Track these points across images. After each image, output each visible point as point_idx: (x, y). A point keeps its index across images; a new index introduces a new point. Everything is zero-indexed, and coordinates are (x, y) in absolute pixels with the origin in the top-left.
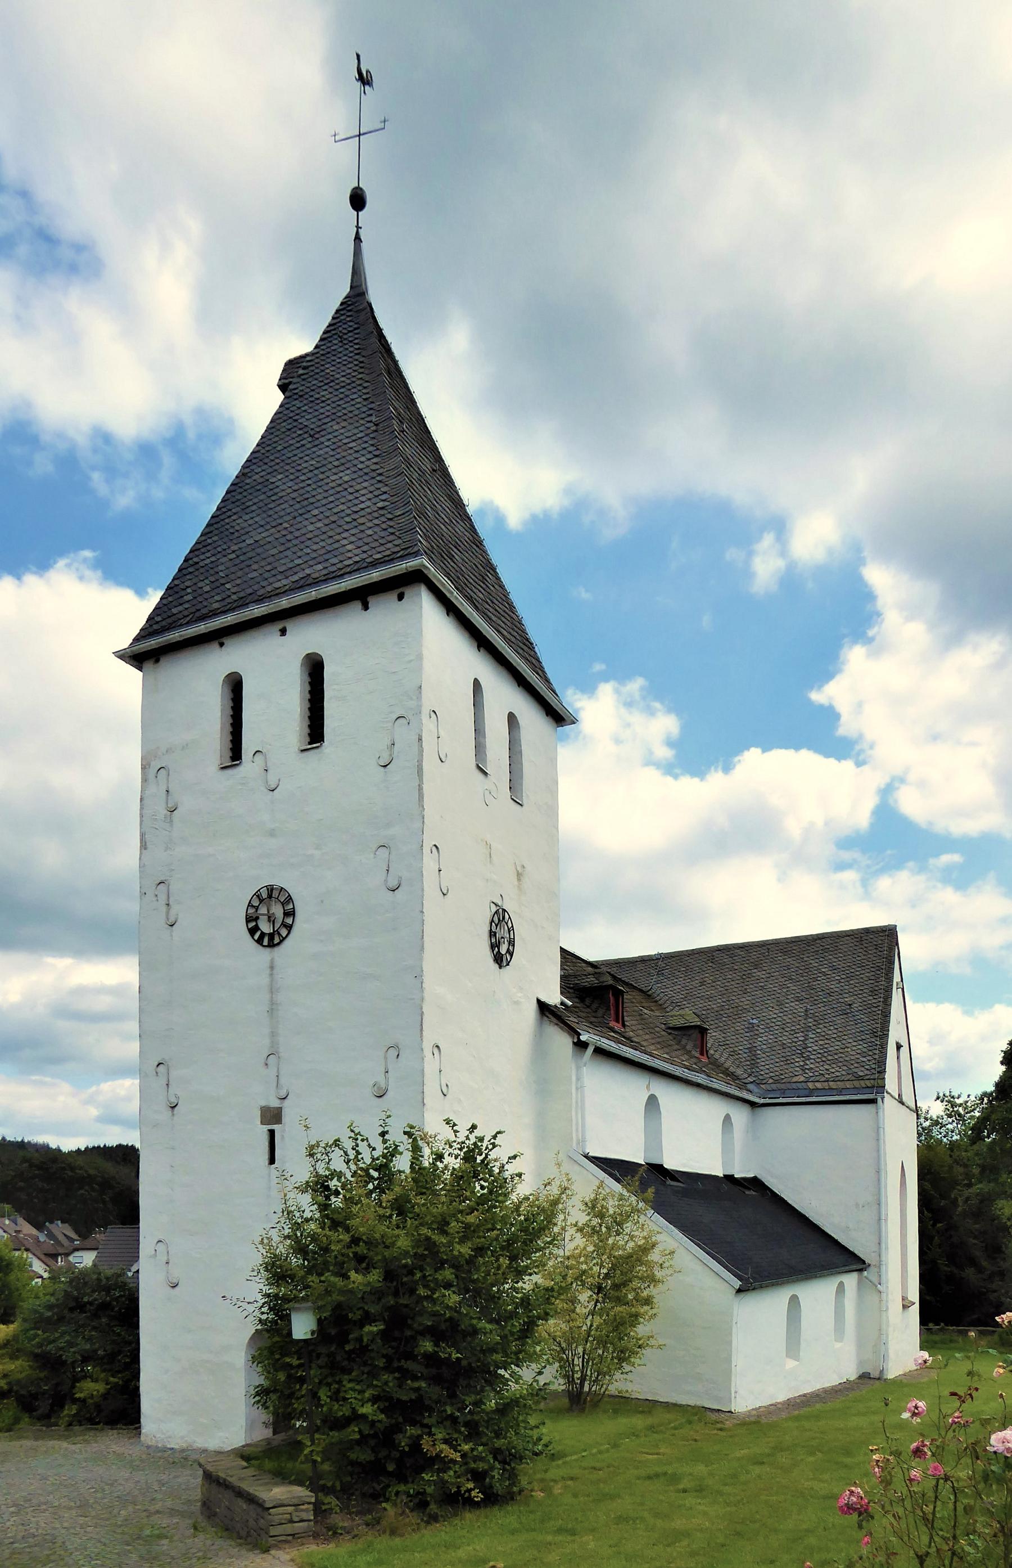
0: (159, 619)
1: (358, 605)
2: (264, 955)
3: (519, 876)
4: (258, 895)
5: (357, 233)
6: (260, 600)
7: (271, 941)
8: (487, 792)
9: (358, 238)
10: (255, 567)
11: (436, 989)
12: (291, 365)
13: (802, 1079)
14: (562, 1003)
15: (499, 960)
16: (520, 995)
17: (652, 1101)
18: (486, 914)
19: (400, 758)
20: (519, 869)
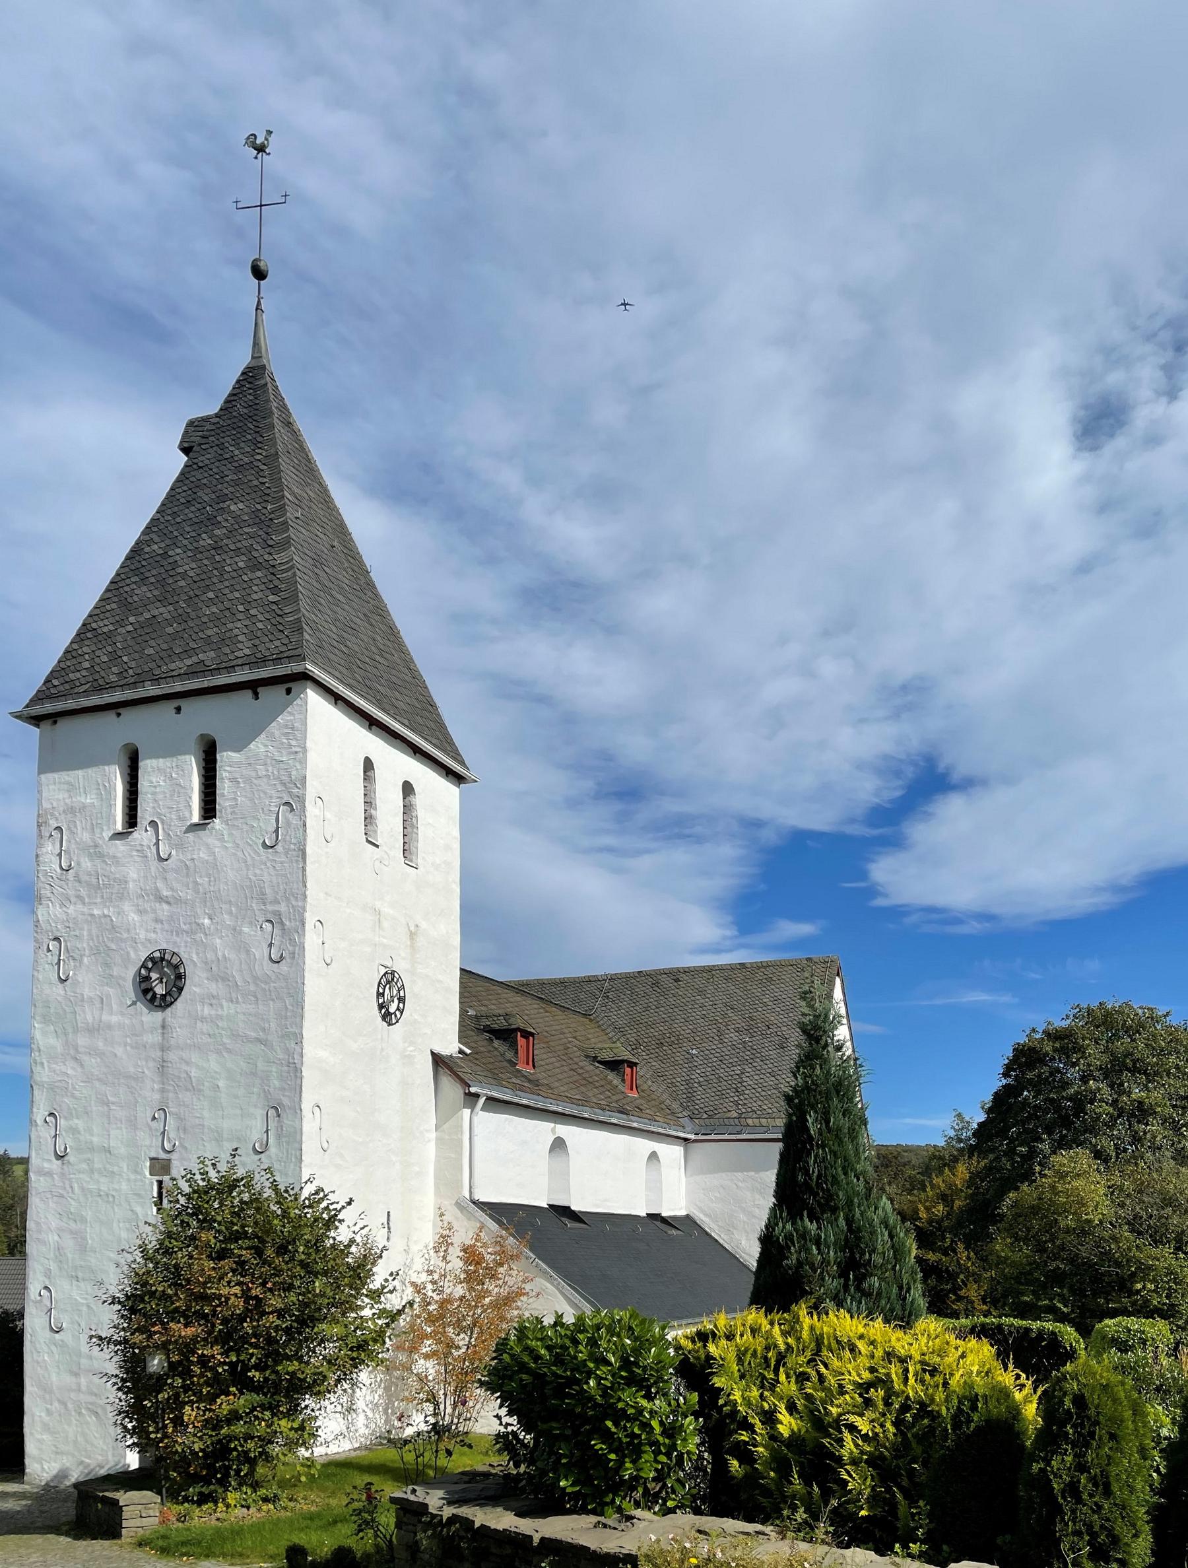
0: (56, 682)
1: (248, 694)
3: (412, 935)
5: (259, 303)
6: (156, 680)
7: (161, 1003)
8: (377, 863)
10: (152, 643)
12: (193, 425)
13: (735, 1115)
14: (461, 1052)
15: (387, 1017)
16: (411, 1048)
17: (559, 1144)
18: (377, 973)
19: (286, 843)
20: (412, 928)
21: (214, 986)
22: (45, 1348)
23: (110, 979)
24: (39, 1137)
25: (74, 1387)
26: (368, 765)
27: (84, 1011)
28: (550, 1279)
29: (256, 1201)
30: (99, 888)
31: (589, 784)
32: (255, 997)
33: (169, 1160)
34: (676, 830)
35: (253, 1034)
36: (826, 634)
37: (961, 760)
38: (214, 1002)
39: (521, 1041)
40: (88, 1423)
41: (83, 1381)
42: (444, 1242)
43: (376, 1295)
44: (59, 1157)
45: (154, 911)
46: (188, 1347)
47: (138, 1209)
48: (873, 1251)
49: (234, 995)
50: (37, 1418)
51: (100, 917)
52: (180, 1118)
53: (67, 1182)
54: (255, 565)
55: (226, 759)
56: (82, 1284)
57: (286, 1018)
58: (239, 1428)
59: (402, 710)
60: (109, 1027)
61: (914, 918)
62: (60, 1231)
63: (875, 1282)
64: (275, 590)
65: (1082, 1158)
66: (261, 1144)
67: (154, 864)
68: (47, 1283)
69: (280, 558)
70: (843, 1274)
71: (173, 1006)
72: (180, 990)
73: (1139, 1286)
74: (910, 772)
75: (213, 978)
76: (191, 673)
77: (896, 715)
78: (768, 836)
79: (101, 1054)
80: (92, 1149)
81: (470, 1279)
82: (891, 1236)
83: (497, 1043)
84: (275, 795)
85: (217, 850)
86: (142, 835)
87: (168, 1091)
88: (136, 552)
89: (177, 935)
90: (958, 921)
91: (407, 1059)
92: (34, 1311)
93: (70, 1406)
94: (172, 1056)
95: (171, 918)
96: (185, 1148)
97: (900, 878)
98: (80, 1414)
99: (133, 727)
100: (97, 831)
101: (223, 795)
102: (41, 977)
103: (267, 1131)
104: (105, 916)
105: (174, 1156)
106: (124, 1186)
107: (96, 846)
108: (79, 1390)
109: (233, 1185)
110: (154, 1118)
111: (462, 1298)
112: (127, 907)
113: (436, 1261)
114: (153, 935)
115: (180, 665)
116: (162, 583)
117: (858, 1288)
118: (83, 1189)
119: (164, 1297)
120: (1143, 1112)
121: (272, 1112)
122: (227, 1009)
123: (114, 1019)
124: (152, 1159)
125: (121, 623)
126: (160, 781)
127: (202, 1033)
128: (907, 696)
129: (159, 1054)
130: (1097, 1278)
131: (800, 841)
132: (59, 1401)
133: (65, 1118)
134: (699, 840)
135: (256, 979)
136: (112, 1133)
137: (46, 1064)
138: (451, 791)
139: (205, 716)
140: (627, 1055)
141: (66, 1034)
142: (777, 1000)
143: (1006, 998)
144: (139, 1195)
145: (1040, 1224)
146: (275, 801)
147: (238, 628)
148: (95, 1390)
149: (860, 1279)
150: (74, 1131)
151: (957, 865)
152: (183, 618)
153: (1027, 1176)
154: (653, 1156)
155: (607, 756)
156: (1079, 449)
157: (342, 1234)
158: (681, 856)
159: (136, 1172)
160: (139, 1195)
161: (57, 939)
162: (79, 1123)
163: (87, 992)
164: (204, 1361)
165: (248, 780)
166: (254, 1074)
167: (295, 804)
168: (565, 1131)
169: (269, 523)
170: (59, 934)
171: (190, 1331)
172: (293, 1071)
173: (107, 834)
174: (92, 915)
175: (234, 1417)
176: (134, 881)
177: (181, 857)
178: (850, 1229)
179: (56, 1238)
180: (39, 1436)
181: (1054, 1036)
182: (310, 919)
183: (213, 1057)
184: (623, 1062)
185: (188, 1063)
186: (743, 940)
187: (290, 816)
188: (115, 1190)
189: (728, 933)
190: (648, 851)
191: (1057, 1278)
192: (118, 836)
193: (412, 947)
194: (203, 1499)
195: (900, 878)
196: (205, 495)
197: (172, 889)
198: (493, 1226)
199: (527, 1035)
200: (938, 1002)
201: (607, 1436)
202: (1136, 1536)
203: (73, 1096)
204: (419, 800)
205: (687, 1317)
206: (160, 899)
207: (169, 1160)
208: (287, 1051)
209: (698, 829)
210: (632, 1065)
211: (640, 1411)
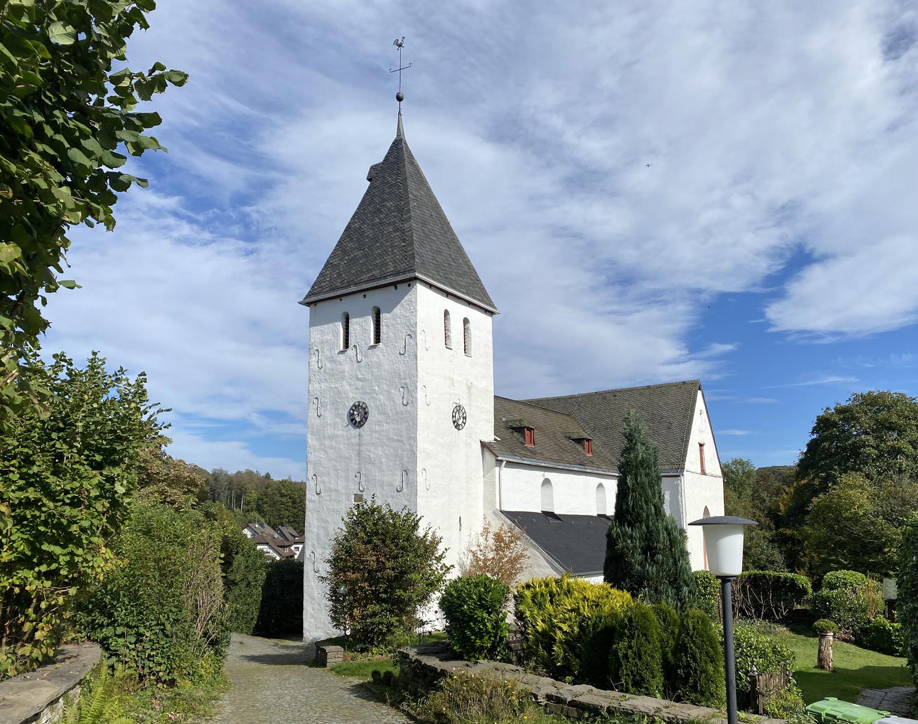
1: (393, 288)
2: (354, 432)
3: (469, 388)
4: (354, 405)
6: (356, 284)
7: (357, 424)
9: (399, 113)
11: (424, 442)
15: (457, 427)
17: (547, 482)
19: (409, 353)
23: (338, 415)
26: (446, 313)
28: (537, 549)
29: (382, 518)
31: (604, 278)
34: (652, 299)
36: (736, 183)
37: (818, 245)
39: (527, 432)
42: (486, 531)
43: (439, 559)
44: (318, 494)
46: (353, 583)
48: (658, 542)
52: (366, 476)
54: (396, 230)
55: (384, 316)
58: (377, 619)
59: (463, 283)
60: (338, 436)
61: (793, 337)
62: (318, 527)
63: (660, 557)
64: (404, 240)
65: (856, 478)
67: (355, 364)
69: (406, 226)
70: (644, 552)
73: (886, 550)
74: (788, 255)
75: (380, 413)
76: (370, 280)
77: (779, 224)
78: (704, 297)
79: (334, 448)
80: (331, 490)
81: (498, 549)
82: (669, 534)
83: (515, 434)
86: (351, 352)
88: (348, 228)
90: (819, 337)
91: (468, 445)
94: (363, 448)
95: (363, 388)
97: (784, 316)
99: (346, 305)
105: (364, 493)
109: (373, 512)
111: (493, 558)
112: (344, 383)
113: (482, 540)
115: (365, 277)
116: (359, 240)
117: (653, 560)
119: (346, 560)
120: (896, 452)
122: (386, 427)
123: (340, 433)
125: (342, 260)
126: (357, 327)
128: (785, 212)
130: (864, 545)
131: (723, 298)
134: (665, 303)
135: (397, 413)
138: (488, 319)
139: (375, 299)
140: (586, 436)
142: (666, 403)
143: (852, 379)
145: (833, 516)
146: (405, 334)
147: (388, 259)
149: (653, 556)
150: (324, 482)
151: (819, 305)
152: (367, 256)
153: (824, 488)
154: (600, 485)
155: (612, 262)
156: (886, 60)
157: (420, 533)
158: (655, 313)
162: (326, 479)
163: (329, 422)
164: (361, 588)
165: (393, 325)
166: (396, 456)
167: (412, 335)
168: (549, 475)
169: (403, 211)
171: (353, 576)
172: (413, 454)
173: (337, 352)
175: (374, 615)
178: (648, 532)
181: (841, 411)
182: (419, 385)
183: (380, 448)
184: (583, 439)
185: (370, 451)
186: (691, 356)
189: (683, 352)
190: (637, 311)
191: (841, 545)
192: (341, 352)
193: (469, 393)
194: (363, 650)
195: (784, 316)
196: (377, 200)
198: (509, 522)
199: (530, 429)
200: (811, 383)
201: (471, 629)
202: (653, 677)
204: (471, 326)
205: (580, 571)
206: (358, 379)
208: (410, 445)
209: (665, 297)
210: (588, 440)
211: (483, 619)
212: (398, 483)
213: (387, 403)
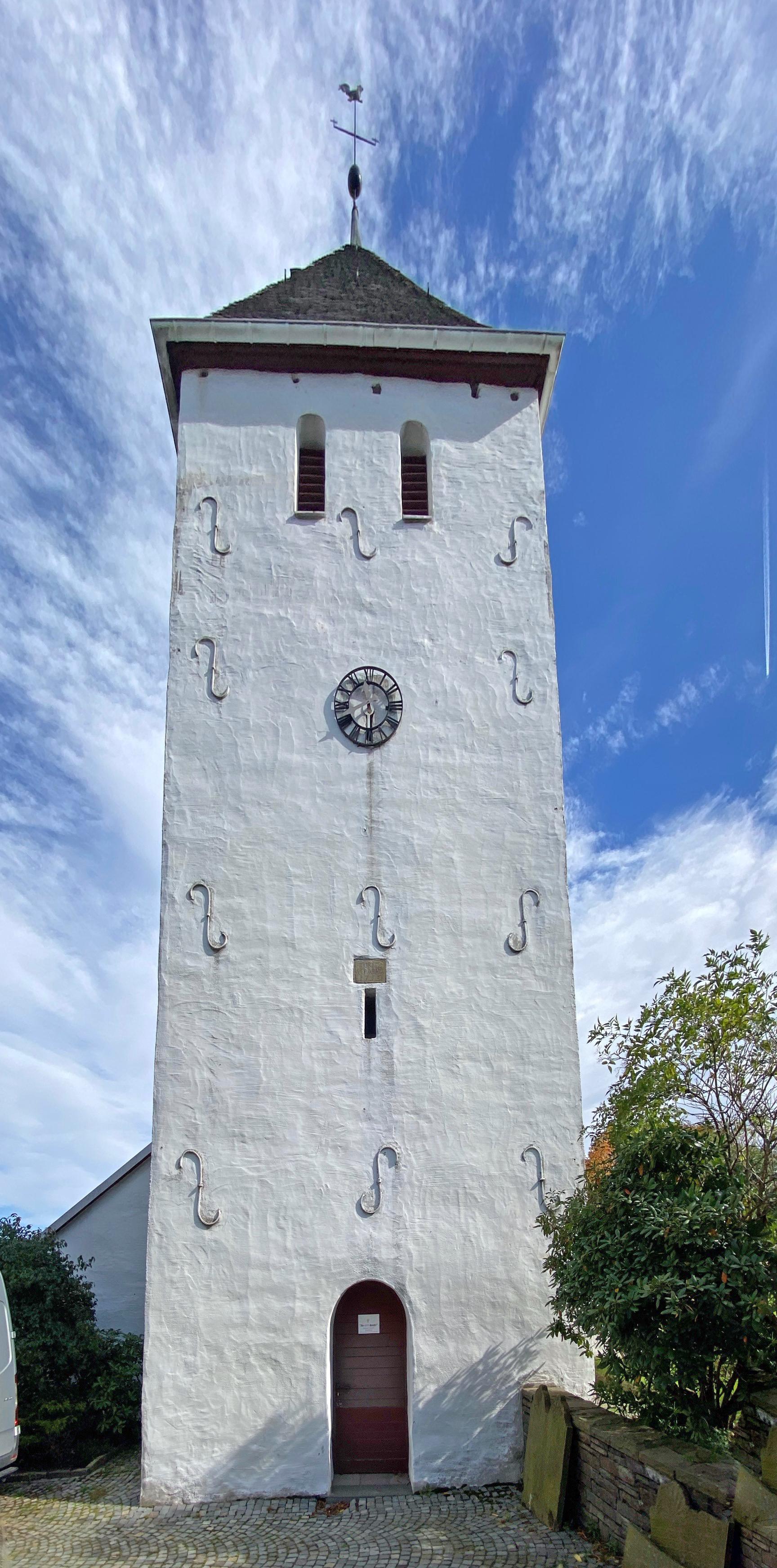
7: (369, 740)
21: (440, 725)
22: (185, 1255)
24: (178, 920)
25: (237, 1319)
27: (249, 744)
30: (272, 582)
32: (498, 746)
33: (384, 961)
35: (497, 794)
38: (441, 746)
40: (259, 1381)
41: (252, 1307)
44: (214, 951)
45: (353, 620)
47: (341, 1031)
49: (468, 741)
50: (166, 1381)
51: (272, 619)
53: (225, 991)
56: (249, 1147)
57: (540, 775)
60: (289, 769)
66: (515, 942)
67: (351, 564)
68: (191, 1148)
71: (384, 748)
72: (394, 725)
84: (507, 506)
85: (437, 556)
87: (379, 864)
89: (386, 656)
92: (166, 1194)
93: (229, 1353)
96: (408, 944)
98: (246, 1366)
100: (267, 511)
101: (441, 495)
102: (180, 690)
103: (523, 922)
104: (281, 618)
105: (392, 955)
106: (317, 996)
107: (265, 529)
108: (246, 1324)
110: (361, 900)
112: (312, 610)
114: (352, 652)
118: (250, 999)
121: (528, 899)
122: (460, 757)
124: (357, 959)
127: (427, 786)
129: (366, 811)
132: (208, 1346)
133: (220, 894)
136: (297, 918)
137: (188, 814)
141: (219, 773)
144: (340, 1010)
148: (277, 1324)
150: (236, 914)
159: (334, 976)
160: (340, 1010)
161: (206, 641)
162: (244, 903)
163: (253, 718)
170: (209, 635)
174: (261, 615)
176: (323, 579)
177: (388, 557)
179: (207, 1074)
180: (170, 1415)
185: (408, 826)
187: (527, 534)
188: (305, 1002)
197: (378, 595)
203: (233, 862)
206: (362, 606)
207: (384, 961)
212: (508, 928)
213: (464, 691)
